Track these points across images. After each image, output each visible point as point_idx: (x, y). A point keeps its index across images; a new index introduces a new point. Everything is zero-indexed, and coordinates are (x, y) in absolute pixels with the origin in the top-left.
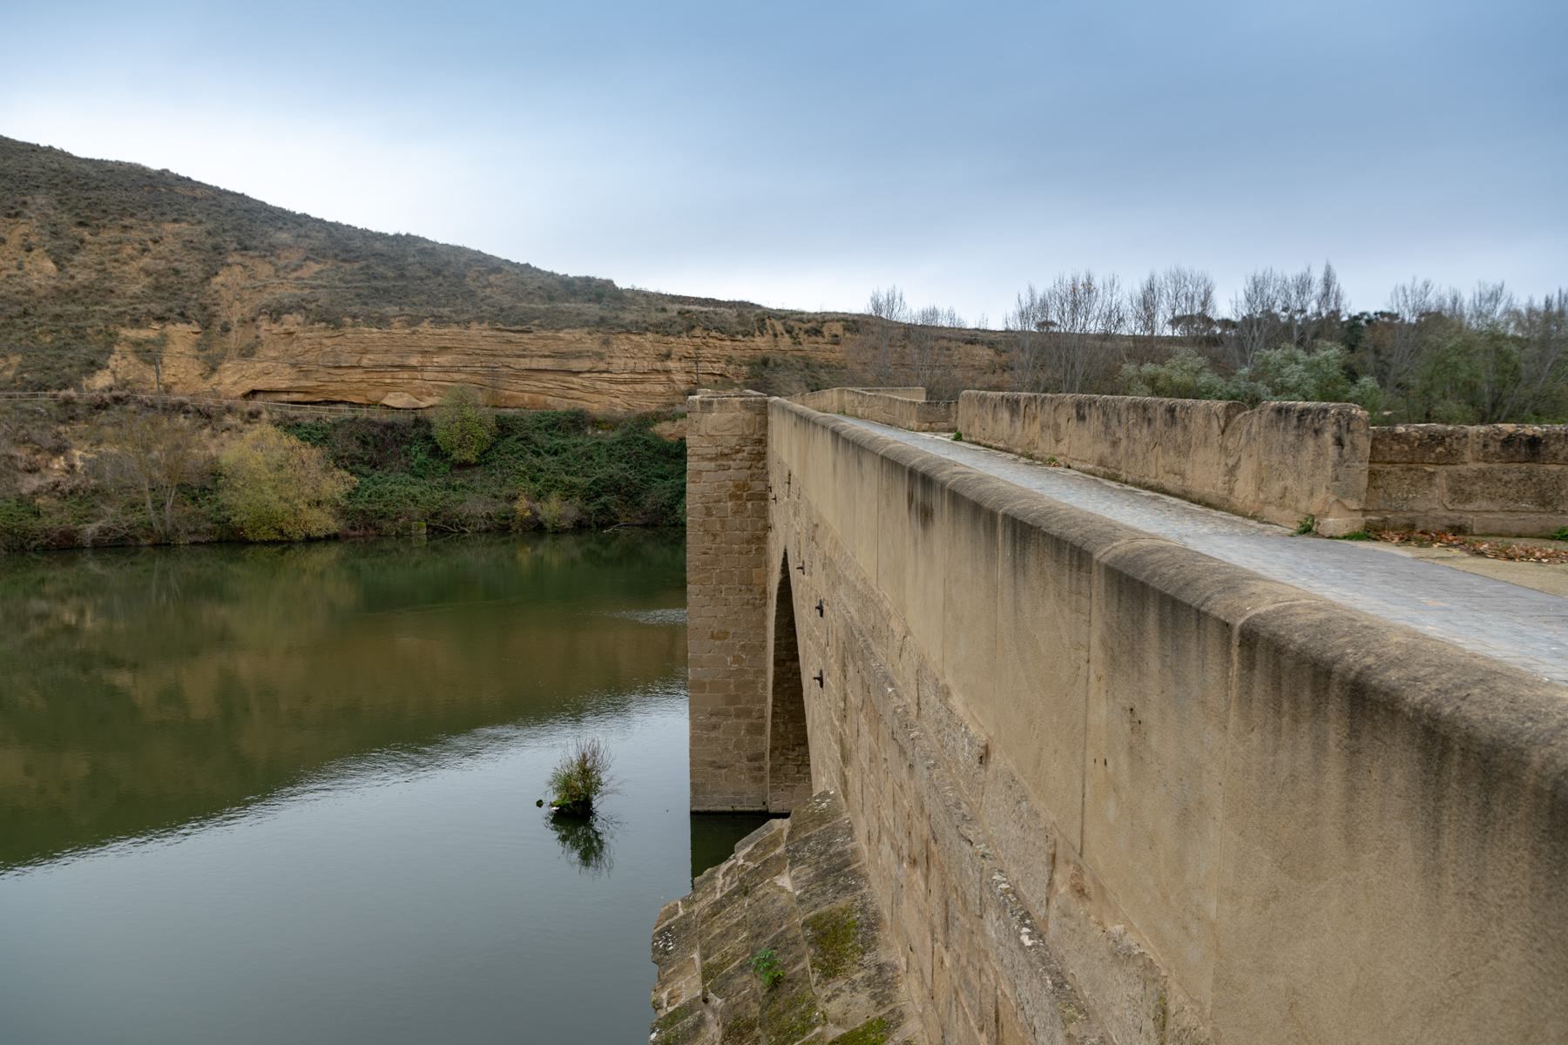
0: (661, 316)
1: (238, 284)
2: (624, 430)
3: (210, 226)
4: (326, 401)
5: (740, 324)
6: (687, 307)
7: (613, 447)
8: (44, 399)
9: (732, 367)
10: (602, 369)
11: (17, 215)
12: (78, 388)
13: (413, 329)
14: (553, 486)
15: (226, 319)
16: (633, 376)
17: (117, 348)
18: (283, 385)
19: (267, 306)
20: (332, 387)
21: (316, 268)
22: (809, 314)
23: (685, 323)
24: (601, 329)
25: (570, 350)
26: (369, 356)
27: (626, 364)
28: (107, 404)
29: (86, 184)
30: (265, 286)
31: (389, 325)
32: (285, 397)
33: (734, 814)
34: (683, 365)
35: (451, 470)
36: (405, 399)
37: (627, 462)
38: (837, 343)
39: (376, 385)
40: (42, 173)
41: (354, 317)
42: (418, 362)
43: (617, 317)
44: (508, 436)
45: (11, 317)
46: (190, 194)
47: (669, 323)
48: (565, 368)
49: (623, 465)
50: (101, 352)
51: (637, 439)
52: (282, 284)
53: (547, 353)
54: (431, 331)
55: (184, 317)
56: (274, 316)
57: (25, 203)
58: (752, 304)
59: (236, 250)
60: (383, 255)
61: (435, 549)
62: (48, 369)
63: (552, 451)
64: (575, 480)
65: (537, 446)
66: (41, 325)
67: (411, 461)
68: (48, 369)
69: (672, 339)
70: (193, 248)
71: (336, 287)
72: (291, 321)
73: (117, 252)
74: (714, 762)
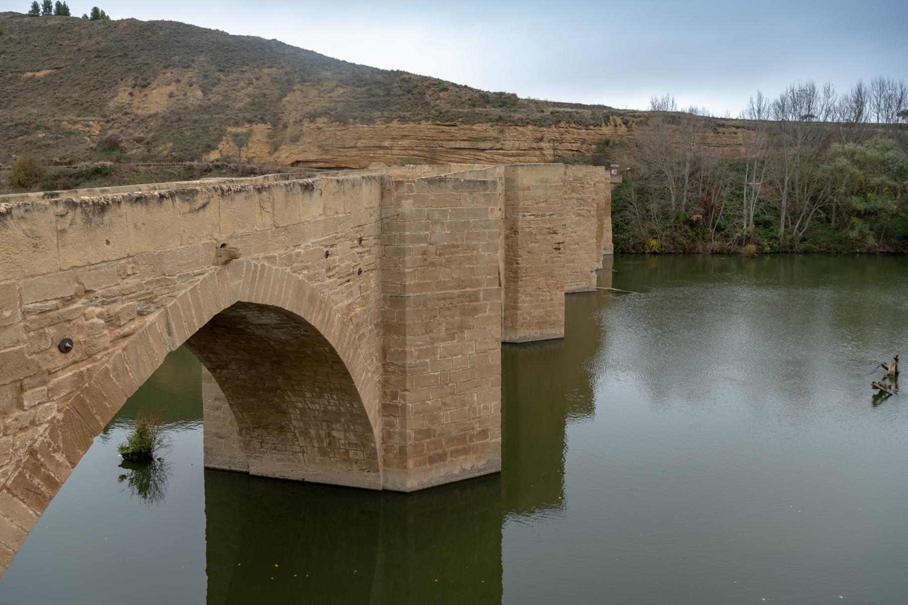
0: (539, 115)
1: (297, 101)
3: (288, 69)
4: (337, 167)
5: (593, 119)
8: (178, 166)
9: (584, 146)
10: (498, 147)
11: (188, 67)
12: (200, 160)
13: (387, 125)
15: (287, 121)
16: (518, 152)
17: (224, 138)
18: (313, 158)
19: (308, 113)
20: (340, 159)
21: (341, 91)
22: (640, 112)
24: (499, 124)
26: (361, 141)
27: (514, 144)
28: (211, 169)
29: (227, 49)
30: (310, 102)
31: (374, 123)
32: (314, 165)
33: (231, 472)
40: (207, 44)
41: (355, 118)
45: (172, 122)
46: (282, 52)
47: (544, 119)
48: (476, 147)
50: (215, 140)
52: (320, 100)
53: (465, 138)
54: (397, 126)
55: (263, 120)
56: (312, 119)
57: (193, 60)
59: (299, 82)
62: (186, 150)
66: (186, 126)
68: (186, 150)
69: (545, 129)
70: (276, 82)
71: (350, 102)
72: (321, 121)
73: (235, 85)
74: (217, 433)
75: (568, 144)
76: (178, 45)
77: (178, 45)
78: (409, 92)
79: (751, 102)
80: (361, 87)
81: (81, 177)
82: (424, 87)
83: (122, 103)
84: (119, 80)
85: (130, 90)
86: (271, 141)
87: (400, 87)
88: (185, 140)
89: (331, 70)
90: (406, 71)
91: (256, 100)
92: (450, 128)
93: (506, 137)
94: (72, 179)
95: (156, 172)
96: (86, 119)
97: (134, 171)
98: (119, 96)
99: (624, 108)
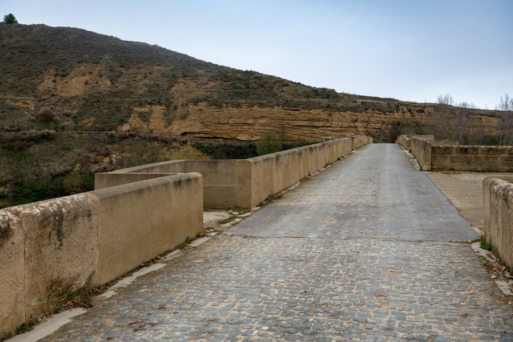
0: (354, 104)
5: (388, 108)
8: (103, 135)
9: (384, 125)
10: (328, 126)
11: (97, 63)
12: (116, 130)
13: (251, 109)
15: (176, 104)
17: (132, 115)
20: (217, 131)
22: (419, 104)
24: (328, 109)
29: (125, 51)
30: (192, 91)
31: (241, 107)
32: (197, 135)
41: (227, 104)
45: (92, 103)
46: (165, 54)
48: (312, 125)
50: (126, 117)
52: (199, 90)
53: (305, 119)
54: (258, 110)
55: (159, 103)
56: (195, 103)
57: (101, 58)
59: (182, 77)
66: (103, 106)
69: (358, 114)
70: (165, 76)
72: (202, 105)
73: (135, 77)
76: (86, 46)
77: (86, 46)
78: (262, 86)
79: (502, 100)
80: (227, 82)
81: (32, 140)
83: (48, 88)
84: (43, 70)
85: (53, 78)
86: (166, 118)
87: (255, 82)
88: (103, 116)
89: (203, 69)
90: (256, 71)
91: (152, 88)
94: (24, 142)
95: (87, 138)
96: (24, 98)
97: (71, 137)
98: (45, 83)
99: (406, 101)
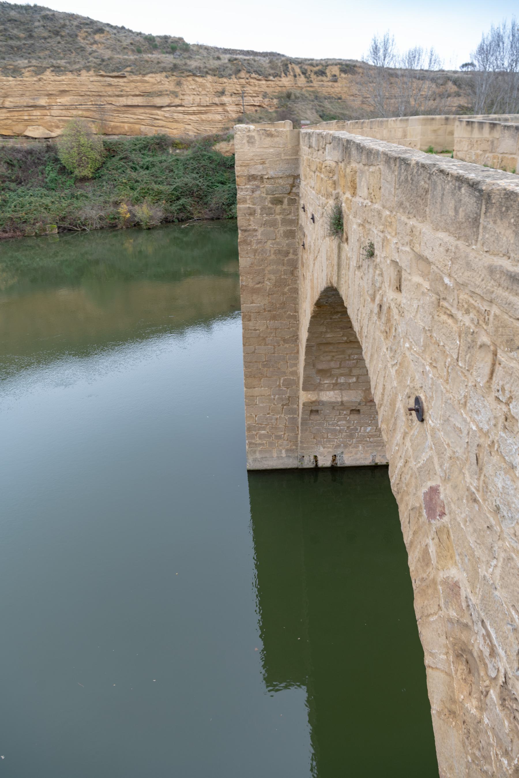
0: (217, 63)
2: (194, 149)
5: (272, 68)
6: (235, 56)
7: (188, 162)
9: (267, 100)
10: (178, 104)
13: (39, 77)
14: (146, 193)
22: (317, 60)
23: (234, 68)
24: (175, 74)
25: (154, 90)
27: (194, 100)
31: (21, 74)
34: (234, 99)
35: (75, 184)
36: (41, 131)
37: (197, 173)
38: (336, 81)
39: (19, 121)
42: (46, 102)
43: (186, 64)
44: (114, 156)
47: (222, 68)
49: (194, 175)
51: (203, 156)
53: (138, 93)
54: (52, 78)
58: (279, 54)
60: (16, 21)
61: (67, 242)
63: (145, 167)
64: (161, 187)
65: (134, 163)
67: (46, 178)
69: (225, 80)
75: (250, 98)
78: (57, 33)
82: (74, 27)
92: (115, 79)
93: (184, 90)
